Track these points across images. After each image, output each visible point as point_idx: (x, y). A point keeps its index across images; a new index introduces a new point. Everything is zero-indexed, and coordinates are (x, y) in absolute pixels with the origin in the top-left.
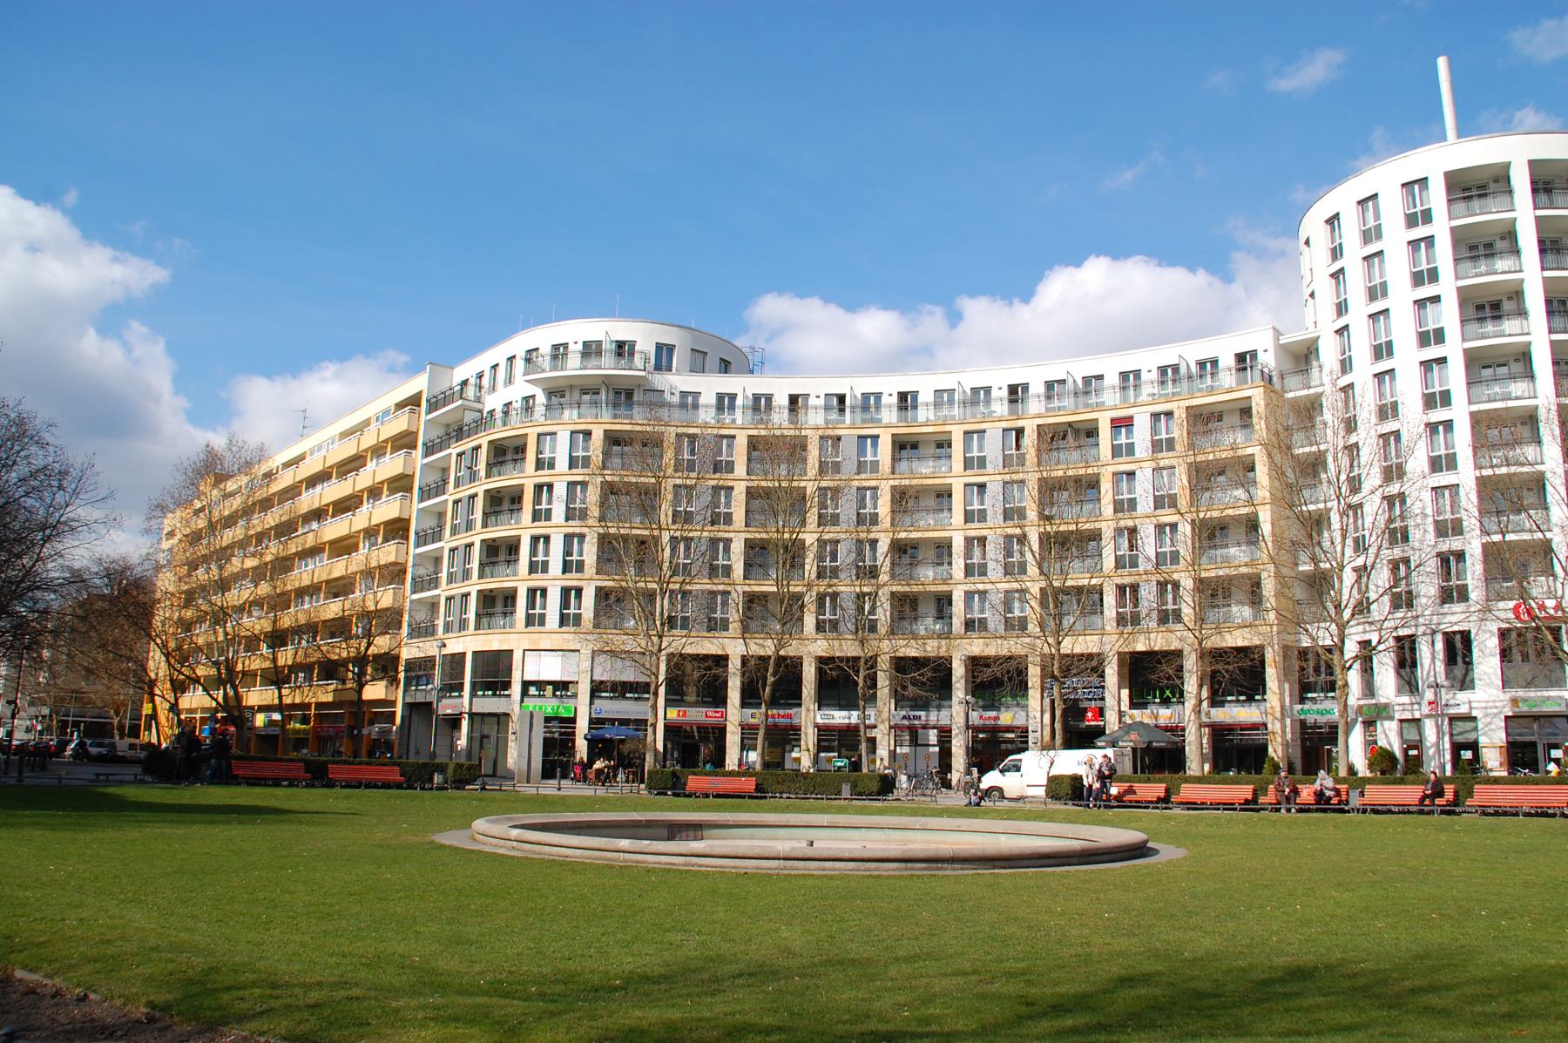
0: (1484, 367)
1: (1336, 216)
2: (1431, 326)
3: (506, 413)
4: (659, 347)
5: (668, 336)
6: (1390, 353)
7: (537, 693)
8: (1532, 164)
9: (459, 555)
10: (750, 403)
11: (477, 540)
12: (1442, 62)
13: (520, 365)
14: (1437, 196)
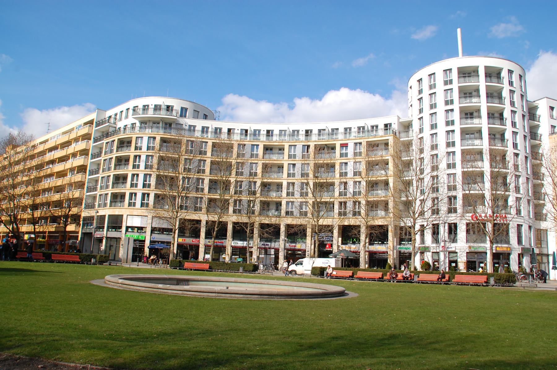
1: (421, 79)
3: (125, 129)
4: (182, 108)
5: (186, 105)
6: (435, 107)
10: (214, 131)
11: (112, 174)
12: (459, 30)
13: (131, 112)
14: (454, 75)
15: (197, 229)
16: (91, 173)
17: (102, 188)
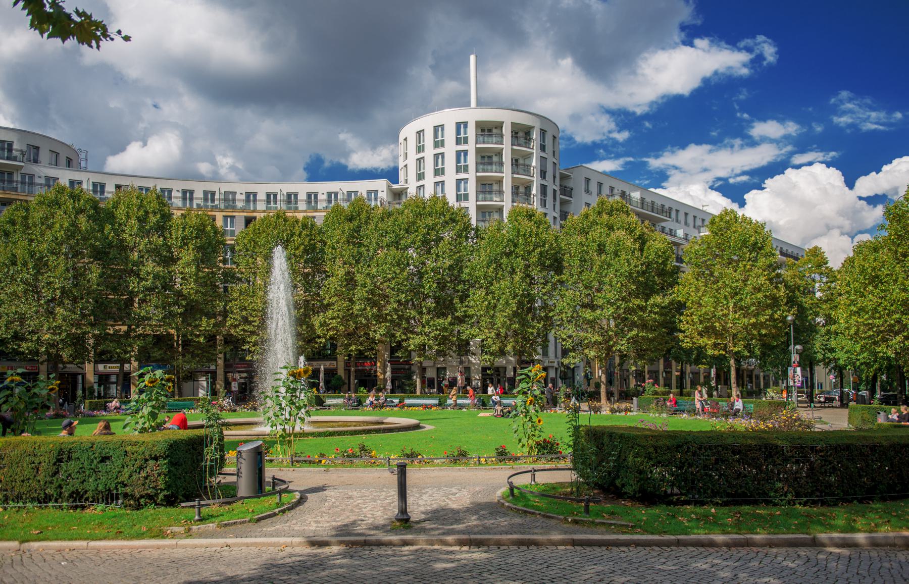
7: (678, 491)
8: (513, 124)
10: (285, 198)
12: (472, 58)
14: (471, 132)
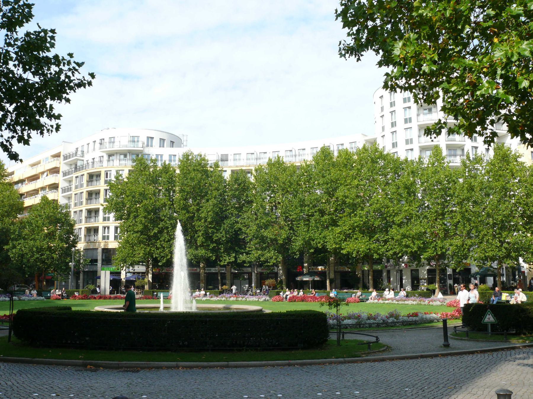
0: (424, 110)
2: (408, 117)
3: (93, 163)
9: (78, 196)
11: (84, 209)
13: (97, 145)
15: (164, 298)
16: (64, 191)
17: (76, 187)
